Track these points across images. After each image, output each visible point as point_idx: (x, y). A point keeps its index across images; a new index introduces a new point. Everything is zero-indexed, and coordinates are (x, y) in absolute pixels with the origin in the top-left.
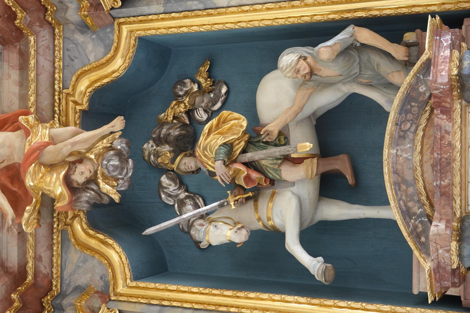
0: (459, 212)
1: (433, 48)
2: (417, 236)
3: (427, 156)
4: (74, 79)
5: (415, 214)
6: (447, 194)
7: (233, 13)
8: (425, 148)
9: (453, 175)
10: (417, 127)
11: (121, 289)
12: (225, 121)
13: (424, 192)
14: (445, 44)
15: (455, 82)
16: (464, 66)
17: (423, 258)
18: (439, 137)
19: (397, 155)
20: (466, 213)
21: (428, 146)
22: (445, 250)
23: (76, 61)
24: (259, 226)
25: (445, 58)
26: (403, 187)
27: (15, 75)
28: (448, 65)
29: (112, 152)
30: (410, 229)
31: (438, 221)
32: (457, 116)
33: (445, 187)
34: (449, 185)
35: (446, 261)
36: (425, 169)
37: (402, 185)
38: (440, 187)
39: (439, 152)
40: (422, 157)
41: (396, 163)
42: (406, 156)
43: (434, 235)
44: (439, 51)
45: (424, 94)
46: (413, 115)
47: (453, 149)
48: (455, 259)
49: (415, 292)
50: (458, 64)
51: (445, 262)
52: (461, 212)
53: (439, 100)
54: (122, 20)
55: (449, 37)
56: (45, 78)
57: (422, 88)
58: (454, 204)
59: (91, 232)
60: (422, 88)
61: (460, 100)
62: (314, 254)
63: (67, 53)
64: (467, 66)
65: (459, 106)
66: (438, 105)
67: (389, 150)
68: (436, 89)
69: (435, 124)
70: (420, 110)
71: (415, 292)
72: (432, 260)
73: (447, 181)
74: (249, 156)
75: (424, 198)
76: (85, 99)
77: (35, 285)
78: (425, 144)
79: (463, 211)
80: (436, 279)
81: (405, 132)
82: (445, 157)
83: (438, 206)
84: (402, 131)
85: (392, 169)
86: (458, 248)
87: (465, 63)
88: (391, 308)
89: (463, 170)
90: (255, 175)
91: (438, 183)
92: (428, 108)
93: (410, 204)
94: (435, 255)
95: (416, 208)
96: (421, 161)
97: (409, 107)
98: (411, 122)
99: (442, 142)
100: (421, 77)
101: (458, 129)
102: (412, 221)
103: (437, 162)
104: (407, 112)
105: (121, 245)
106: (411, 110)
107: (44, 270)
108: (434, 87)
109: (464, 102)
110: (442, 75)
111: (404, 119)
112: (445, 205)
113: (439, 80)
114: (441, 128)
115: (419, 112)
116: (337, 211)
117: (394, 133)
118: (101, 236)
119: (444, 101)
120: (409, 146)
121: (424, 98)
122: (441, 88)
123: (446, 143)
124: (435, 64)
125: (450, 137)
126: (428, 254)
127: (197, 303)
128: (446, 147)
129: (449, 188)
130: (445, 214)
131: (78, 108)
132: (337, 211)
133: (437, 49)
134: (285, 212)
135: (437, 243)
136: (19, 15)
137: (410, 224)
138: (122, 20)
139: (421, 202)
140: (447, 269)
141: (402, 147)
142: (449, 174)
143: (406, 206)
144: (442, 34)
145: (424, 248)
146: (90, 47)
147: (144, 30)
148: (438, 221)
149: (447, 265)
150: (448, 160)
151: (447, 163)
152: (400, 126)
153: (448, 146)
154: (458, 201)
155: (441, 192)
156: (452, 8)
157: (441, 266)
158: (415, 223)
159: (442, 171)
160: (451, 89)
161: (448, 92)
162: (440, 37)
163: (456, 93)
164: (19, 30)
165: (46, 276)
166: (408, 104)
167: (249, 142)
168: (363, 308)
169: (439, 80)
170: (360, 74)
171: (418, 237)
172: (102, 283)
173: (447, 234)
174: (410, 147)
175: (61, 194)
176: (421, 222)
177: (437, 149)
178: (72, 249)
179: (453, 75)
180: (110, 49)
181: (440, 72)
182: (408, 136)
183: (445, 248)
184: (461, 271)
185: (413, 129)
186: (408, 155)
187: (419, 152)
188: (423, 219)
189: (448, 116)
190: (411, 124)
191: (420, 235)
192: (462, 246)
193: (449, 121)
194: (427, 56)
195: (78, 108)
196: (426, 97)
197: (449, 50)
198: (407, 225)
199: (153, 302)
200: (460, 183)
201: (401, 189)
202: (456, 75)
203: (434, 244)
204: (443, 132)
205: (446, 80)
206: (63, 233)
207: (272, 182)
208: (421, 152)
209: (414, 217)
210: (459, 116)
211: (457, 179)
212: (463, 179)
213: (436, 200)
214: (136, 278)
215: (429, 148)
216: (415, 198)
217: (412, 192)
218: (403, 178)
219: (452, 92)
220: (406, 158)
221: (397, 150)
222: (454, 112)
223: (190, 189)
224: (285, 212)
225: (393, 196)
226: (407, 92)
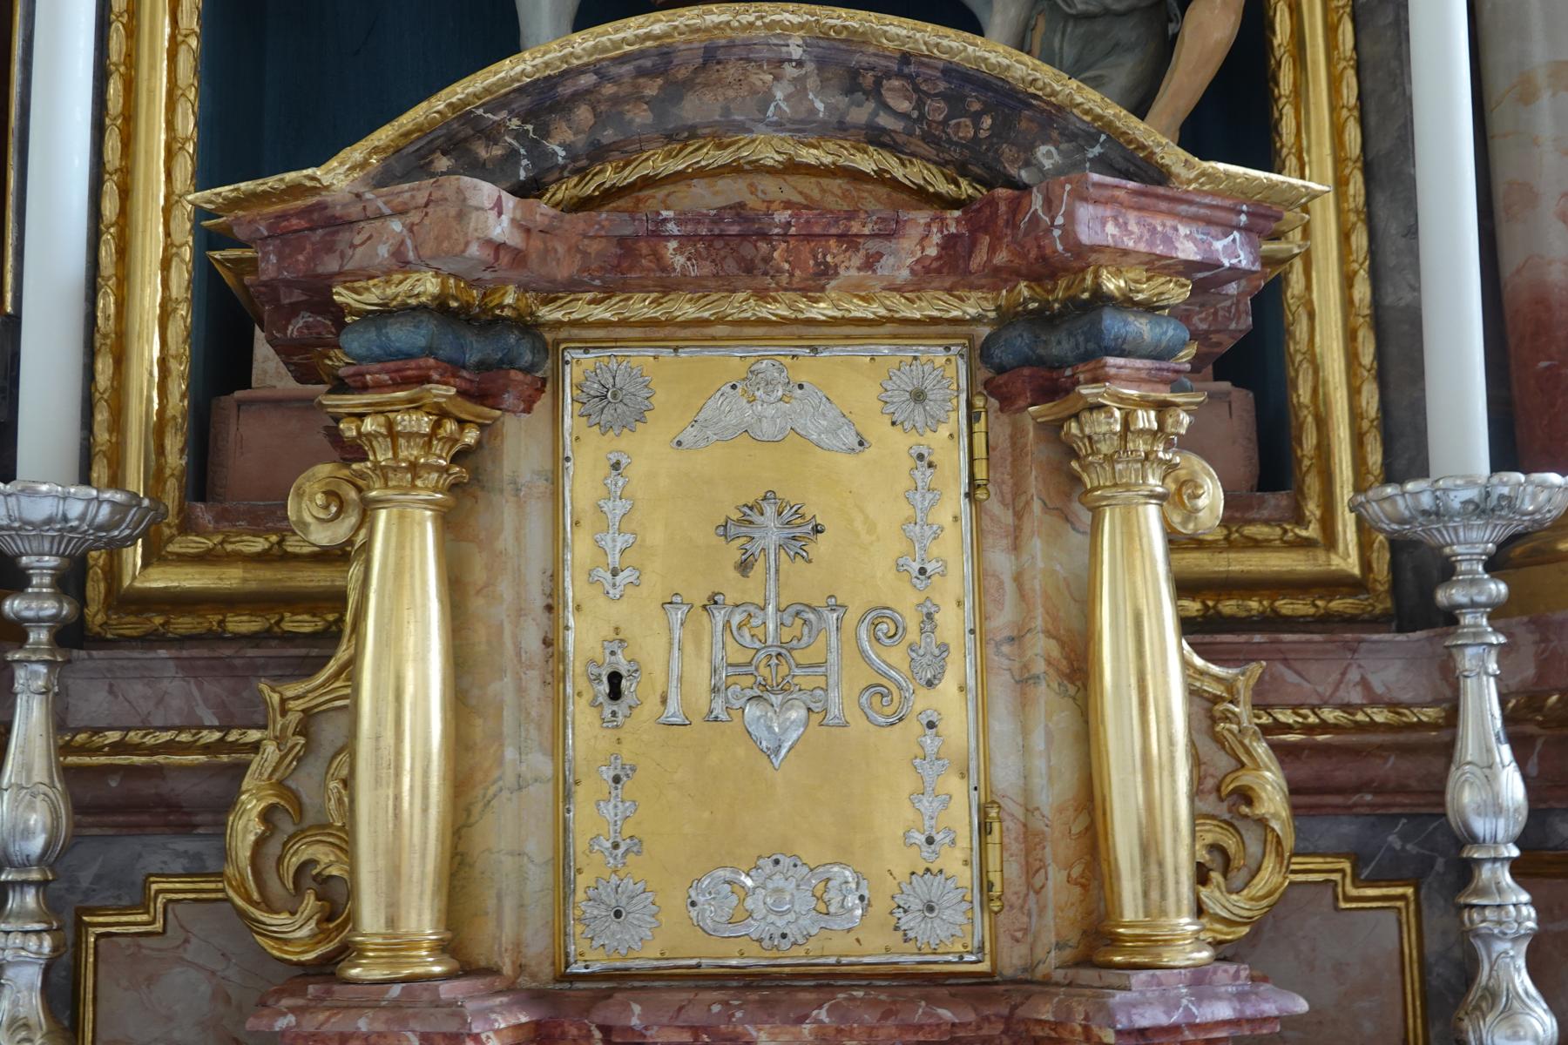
0: (558, 315)
1: (1207, 193)
5: (544, 132)
6: (626, 266)
8: (809, 185)
10: (894, 148)
13: (631, 175)
14: (1219, 245)
15: (1068, 288)
16: (1131, 318)
17: (364, 164)
18: (855, 228)
19: (782, 62)
20: (557, 343)
21: (816, 194)
22: (402, 243)
25: (1168, 241)
26: (652, 88)
28: (1142, 247)
30: (480, 112)
31: (518, 215)
33: (658, 258)
34: (664, 269)
35: (360, 250)
36: (722, 184)
37: (660, 81)
38: (657, 234)
39: (793, 230)
40: (771, 171)
41: (748, 60)
42: (779, 95)
43: (459, 191)
44: (1194, 219)
45: (1027, 164)
46: (945, 122)
47: (804, 291)
50: (1140, 297)
51: (353, 246)
52: (558, 324)
53: (1001, 222)
55: (1244, 263)
57: (1049, 155)
58: (589, 296)
60: (1049, 155)
61: (992, 315)
64: (1130, 328)
65: (972, 311)
66: (979, 218)
67: (801, 26)
68: (1049, 203)
69: (904, 215)
70: (963, 146)
72: (358, 196)
73: (679, 260)
75: (609, 176)
78: (825, 182)
79: (563, 334)
80: (284, 216)
81: (876, 92)
82: (776, 255)
83: (581, 226)
84: (878, 83)
85: (723, 42)
86: (413, 302)
87: (1144, 321)
88: (187, 139)
89: (720, 330)
91: (672, 227)
92: (966, 189)
93: (583, 114)
94: (380, 203)
95: (569, 136)
96: (758, 168)
97: (976, 107)
98: (915, 114)
99: (832, 242)
100: (1097, 150)
101: (883, 312)
102: (515, 123)
103: (753, 221)
104: (955, 102)
106: (966, 114)
108: (1057, 188)
109: (984, 331)
110: (1104, 224)
111: (924, 87)
112: (585, 254)
113: (1085, 212)
114: (890, 236)
115: (957, 144)
117: (871, 50)
119: (1000, 239)
120: (820, 106)
121: (1013, 162)
122: (1053, 219)
123: (829, 259)
124: (1144, 200)
125: (853, 272)
128: (815, 257)
129: (650, 270)
130: (546, 251)
133: (1202, 211)
135: (430, 210)
137: (504, 114)
139: (591, 165)
140: (326, 258)
141: (812, 82)
142: (707, 268)
143: (578, 97)
144: (1255, 236)
145: (410, 163)
148: (518, 215)
149: (342, 256)
150: (762, 266)
151: (752, 260)
152: (900, 75)
153: (818, 264)
154: (600, 313)
155: (637, 238)
156: (1296, 343)
157: (337, 232)
158: (510, 131)
159: (719, 244)
160: (1044, 270)
161: (1033, 255)
162: (1245, 230)
163: (1026, 293)
166: (985, 103)
168: (180, 38)
169: (1085, 212)
170: (1067, 17)
173: (467, 244)
174: (814, 111)
176: (512, 155)
177: (808, 222)
179: (1097, 276)
181: (1115, 218)
182: (859, 105)
183: (409, 242)
184: (332, 353)
185: (884, 120)
186: (784, 106)
187: (791, 159)
188: (525, 162)
189: (935, 265)
190: (904, 116)
191: (459, 143)
192: (425, 317)
193: (918, 268)
194: (1177, 169)
196: (1013, 171)
197: (1198, 258)
198: (500, 102)
200: (670, 322)
201: (641, 80)
202: (1097, 287)
203: (421, 198)
204: (873, 246)
205: (1085, 236)
208: (793, 168)
209: (530, 127)
210: (936, 314)
211: (686, 309)
212: (688, 332)
215: (806, 197)
216: (609, 132)
217: (631, 121)
218: (688, 85)
219: (1026, 278)
220: (768, 98)
221: (800, 64)
222: (949, 291)
225: (616, 45)
226: (1035, 97)
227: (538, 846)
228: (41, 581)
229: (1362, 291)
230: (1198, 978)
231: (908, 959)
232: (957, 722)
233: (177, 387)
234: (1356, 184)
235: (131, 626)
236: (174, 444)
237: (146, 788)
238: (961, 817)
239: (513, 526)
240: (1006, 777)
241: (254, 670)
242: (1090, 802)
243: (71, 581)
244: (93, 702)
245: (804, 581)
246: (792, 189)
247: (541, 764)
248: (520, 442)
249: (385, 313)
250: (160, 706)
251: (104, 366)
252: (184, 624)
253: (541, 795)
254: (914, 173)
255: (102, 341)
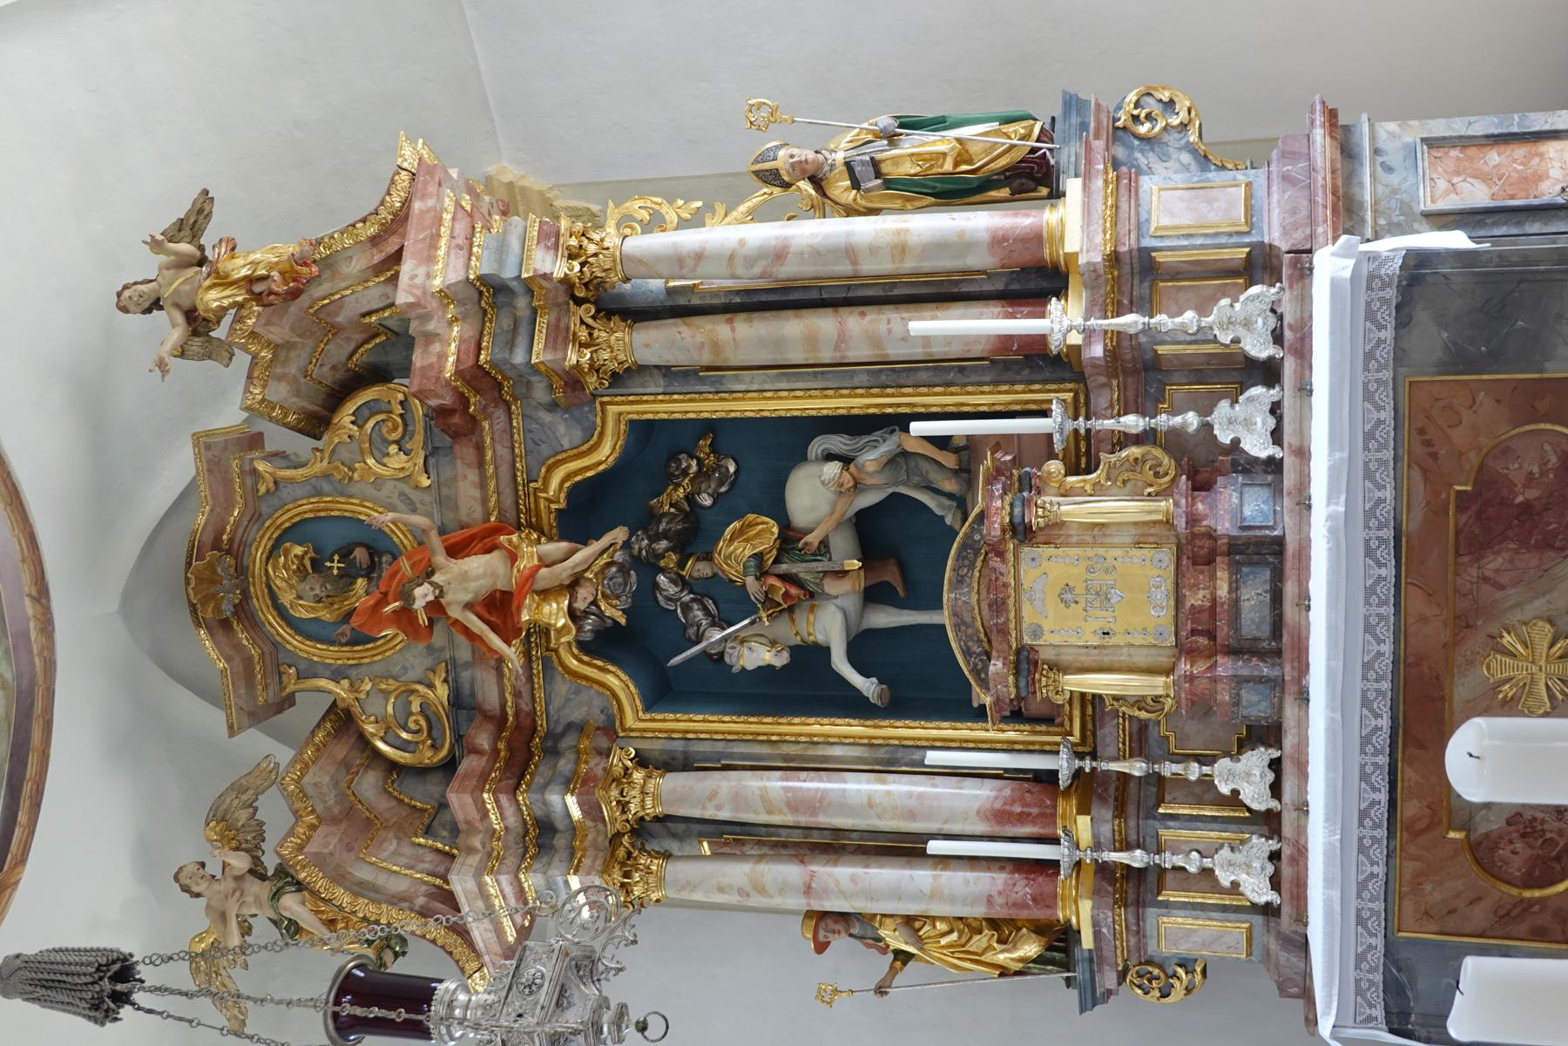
2: (976, 672)
3: (983, 593)
4: (543, 470)
6: (1003, 631)
7: (753, 399)
9: (1008, 611)
11: (630, 722)
12: (751, 525)
23: (543, 446)
24: (798, 641)
27: (473, 476)
29: (614, 569)
32: (1010, 556)
48: (1013, 690)
49: (975, 705)
54: (606, 399)
56: (505, 469)
59: (586, 658)
62: (866, 675)
63: (529, 435)
71: (975, 705)
74: (783, 568)
76: (563, 496)
77: (518, 727)
90: (793, 591)
104: (964, 558)
105: (621, 667)
107: (525, 707)
116: (885, 618)
118: (599, 663)
126: (988, 689)
127: (730, 733)
131: (554, 506)
132: (885, 618)
134: (829, 626)
136: (472, 400)
138: (606, 399)
146: (562, 429)
147: (638, 413)
164: (473, 418)
165: (528, 714)
167: (780, 550)
171: (978, 673)
172: (603, 717)
175: (564, 626)
178: (559, 679)
180: (591, 437)
195: (554, 506)
198: (968, 663)
199: (675, 736)
206: (546, 662)
207: (812, 595)
213: (993, 637)
214: (647, 709)
223: (696, 589)
224: (829, 626)
227: (1145, 651)
228: (1081, 764)
229: (986, 388)
230: (1176, 504)
231: (1172, 567)
232: (1118, 552)
233: (1022, 727)
234: (952, 389)
235: (1090, 740)
236: (1038, 728)
237: (1135, 737)
238: (1138, 552)
239: (1066, 657)
240: (1128, 540)
241: (1103, 710)
242: (1136, 523)
243: (1080, 756)
244: (1111, 750)
245: (1080, 588)
246: (983, 593)
247: (1125, 651)
248: (1046, 654)
249: (1017, 686)
250: (1110, 735)
251: (1017, 747)
252: (1090, 726)
253: (1132, 651)
254: (979, 564)
255: (1028, 750)
